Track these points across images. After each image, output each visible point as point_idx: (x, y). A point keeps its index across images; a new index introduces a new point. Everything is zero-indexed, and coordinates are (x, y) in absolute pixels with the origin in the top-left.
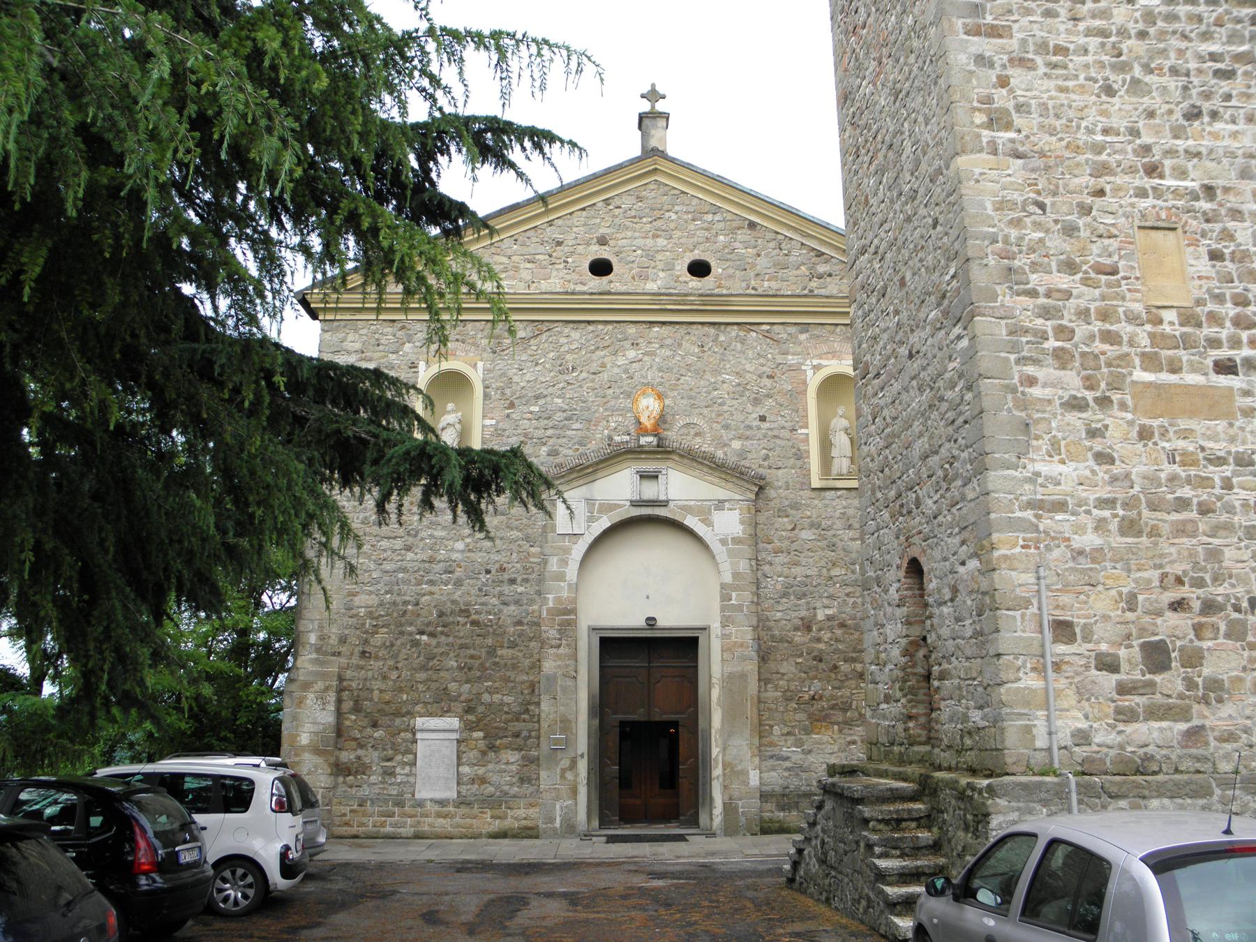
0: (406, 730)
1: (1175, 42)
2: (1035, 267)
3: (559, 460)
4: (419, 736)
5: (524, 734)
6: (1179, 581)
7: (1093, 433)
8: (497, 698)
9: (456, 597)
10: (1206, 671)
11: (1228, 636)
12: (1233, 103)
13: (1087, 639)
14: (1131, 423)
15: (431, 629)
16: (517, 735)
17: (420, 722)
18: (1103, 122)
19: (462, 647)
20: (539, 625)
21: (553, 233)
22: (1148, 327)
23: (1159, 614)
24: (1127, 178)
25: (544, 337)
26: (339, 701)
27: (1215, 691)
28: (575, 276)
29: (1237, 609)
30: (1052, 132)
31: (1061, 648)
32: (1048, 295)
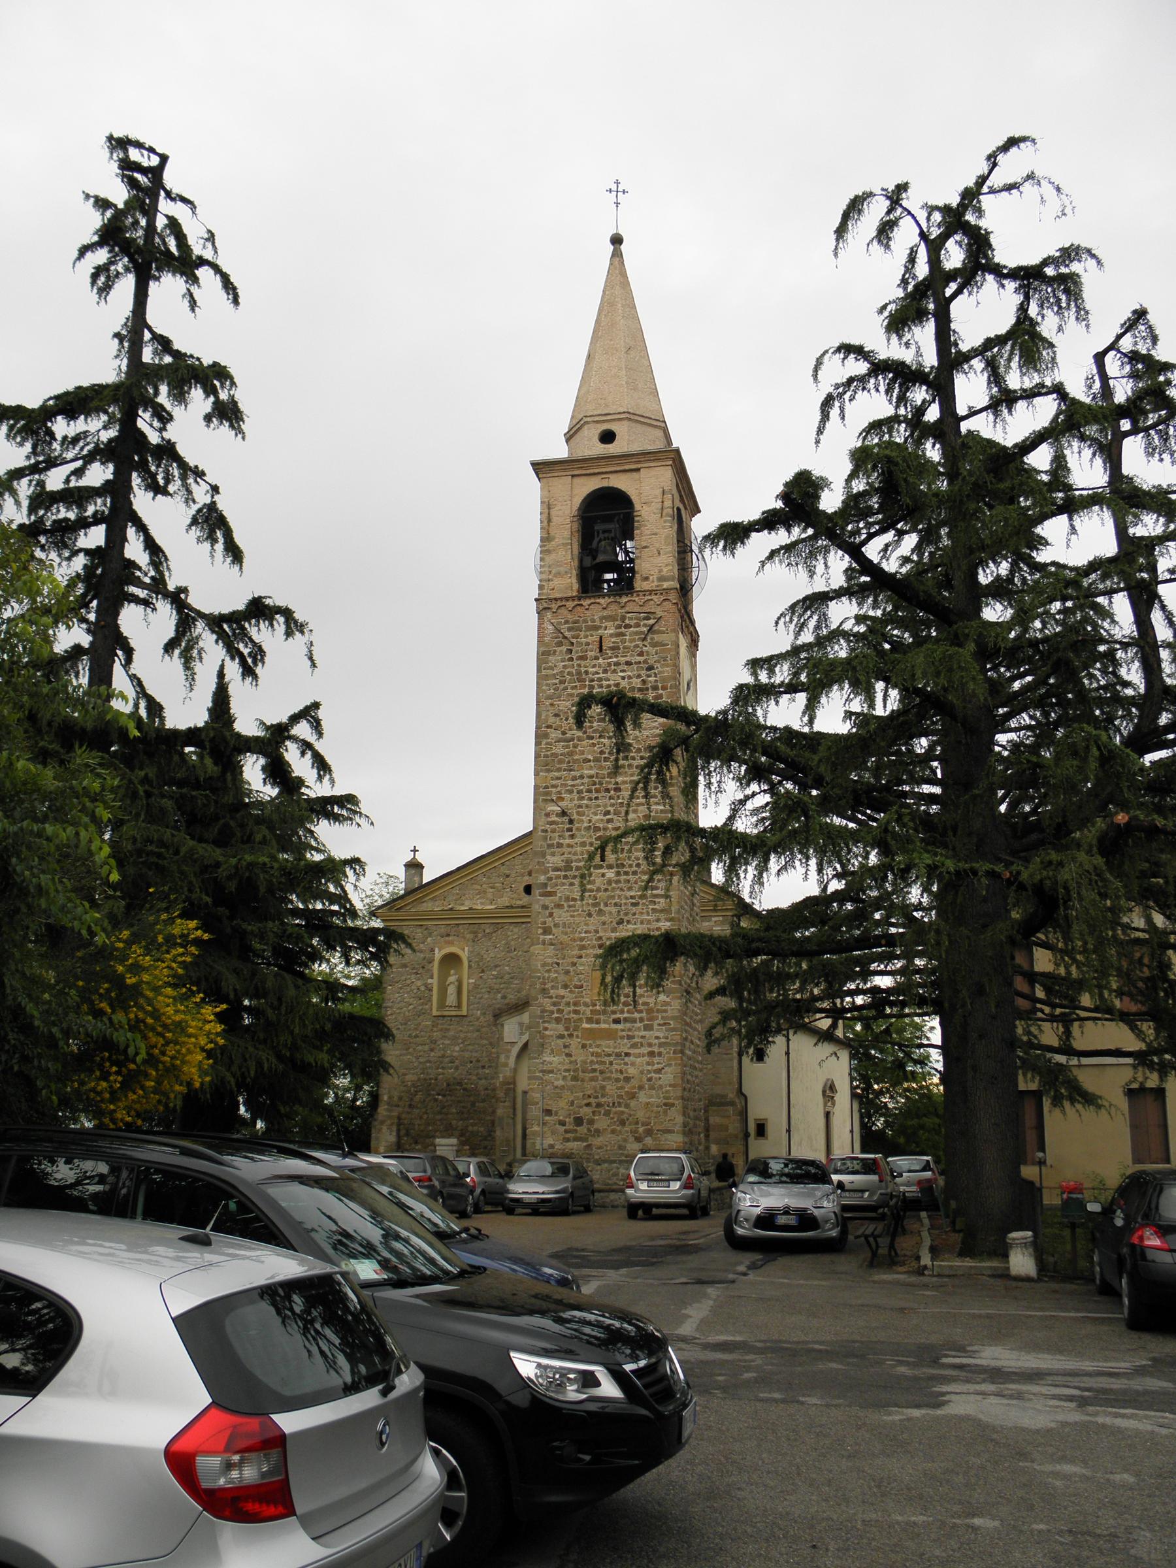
1: (618, 892)
2: (553, 987)
3: (507, 1001)
6: (589, 1097)
7: (565, 1047)
8: (475, 1128)
9: (456, 1075)
16: (485, 1148)
17: (438, 1141)
26: (398, 1131)
27: (598, 1132)
28: (515, 896)
30: (566, 934)
31: (547, 1118)
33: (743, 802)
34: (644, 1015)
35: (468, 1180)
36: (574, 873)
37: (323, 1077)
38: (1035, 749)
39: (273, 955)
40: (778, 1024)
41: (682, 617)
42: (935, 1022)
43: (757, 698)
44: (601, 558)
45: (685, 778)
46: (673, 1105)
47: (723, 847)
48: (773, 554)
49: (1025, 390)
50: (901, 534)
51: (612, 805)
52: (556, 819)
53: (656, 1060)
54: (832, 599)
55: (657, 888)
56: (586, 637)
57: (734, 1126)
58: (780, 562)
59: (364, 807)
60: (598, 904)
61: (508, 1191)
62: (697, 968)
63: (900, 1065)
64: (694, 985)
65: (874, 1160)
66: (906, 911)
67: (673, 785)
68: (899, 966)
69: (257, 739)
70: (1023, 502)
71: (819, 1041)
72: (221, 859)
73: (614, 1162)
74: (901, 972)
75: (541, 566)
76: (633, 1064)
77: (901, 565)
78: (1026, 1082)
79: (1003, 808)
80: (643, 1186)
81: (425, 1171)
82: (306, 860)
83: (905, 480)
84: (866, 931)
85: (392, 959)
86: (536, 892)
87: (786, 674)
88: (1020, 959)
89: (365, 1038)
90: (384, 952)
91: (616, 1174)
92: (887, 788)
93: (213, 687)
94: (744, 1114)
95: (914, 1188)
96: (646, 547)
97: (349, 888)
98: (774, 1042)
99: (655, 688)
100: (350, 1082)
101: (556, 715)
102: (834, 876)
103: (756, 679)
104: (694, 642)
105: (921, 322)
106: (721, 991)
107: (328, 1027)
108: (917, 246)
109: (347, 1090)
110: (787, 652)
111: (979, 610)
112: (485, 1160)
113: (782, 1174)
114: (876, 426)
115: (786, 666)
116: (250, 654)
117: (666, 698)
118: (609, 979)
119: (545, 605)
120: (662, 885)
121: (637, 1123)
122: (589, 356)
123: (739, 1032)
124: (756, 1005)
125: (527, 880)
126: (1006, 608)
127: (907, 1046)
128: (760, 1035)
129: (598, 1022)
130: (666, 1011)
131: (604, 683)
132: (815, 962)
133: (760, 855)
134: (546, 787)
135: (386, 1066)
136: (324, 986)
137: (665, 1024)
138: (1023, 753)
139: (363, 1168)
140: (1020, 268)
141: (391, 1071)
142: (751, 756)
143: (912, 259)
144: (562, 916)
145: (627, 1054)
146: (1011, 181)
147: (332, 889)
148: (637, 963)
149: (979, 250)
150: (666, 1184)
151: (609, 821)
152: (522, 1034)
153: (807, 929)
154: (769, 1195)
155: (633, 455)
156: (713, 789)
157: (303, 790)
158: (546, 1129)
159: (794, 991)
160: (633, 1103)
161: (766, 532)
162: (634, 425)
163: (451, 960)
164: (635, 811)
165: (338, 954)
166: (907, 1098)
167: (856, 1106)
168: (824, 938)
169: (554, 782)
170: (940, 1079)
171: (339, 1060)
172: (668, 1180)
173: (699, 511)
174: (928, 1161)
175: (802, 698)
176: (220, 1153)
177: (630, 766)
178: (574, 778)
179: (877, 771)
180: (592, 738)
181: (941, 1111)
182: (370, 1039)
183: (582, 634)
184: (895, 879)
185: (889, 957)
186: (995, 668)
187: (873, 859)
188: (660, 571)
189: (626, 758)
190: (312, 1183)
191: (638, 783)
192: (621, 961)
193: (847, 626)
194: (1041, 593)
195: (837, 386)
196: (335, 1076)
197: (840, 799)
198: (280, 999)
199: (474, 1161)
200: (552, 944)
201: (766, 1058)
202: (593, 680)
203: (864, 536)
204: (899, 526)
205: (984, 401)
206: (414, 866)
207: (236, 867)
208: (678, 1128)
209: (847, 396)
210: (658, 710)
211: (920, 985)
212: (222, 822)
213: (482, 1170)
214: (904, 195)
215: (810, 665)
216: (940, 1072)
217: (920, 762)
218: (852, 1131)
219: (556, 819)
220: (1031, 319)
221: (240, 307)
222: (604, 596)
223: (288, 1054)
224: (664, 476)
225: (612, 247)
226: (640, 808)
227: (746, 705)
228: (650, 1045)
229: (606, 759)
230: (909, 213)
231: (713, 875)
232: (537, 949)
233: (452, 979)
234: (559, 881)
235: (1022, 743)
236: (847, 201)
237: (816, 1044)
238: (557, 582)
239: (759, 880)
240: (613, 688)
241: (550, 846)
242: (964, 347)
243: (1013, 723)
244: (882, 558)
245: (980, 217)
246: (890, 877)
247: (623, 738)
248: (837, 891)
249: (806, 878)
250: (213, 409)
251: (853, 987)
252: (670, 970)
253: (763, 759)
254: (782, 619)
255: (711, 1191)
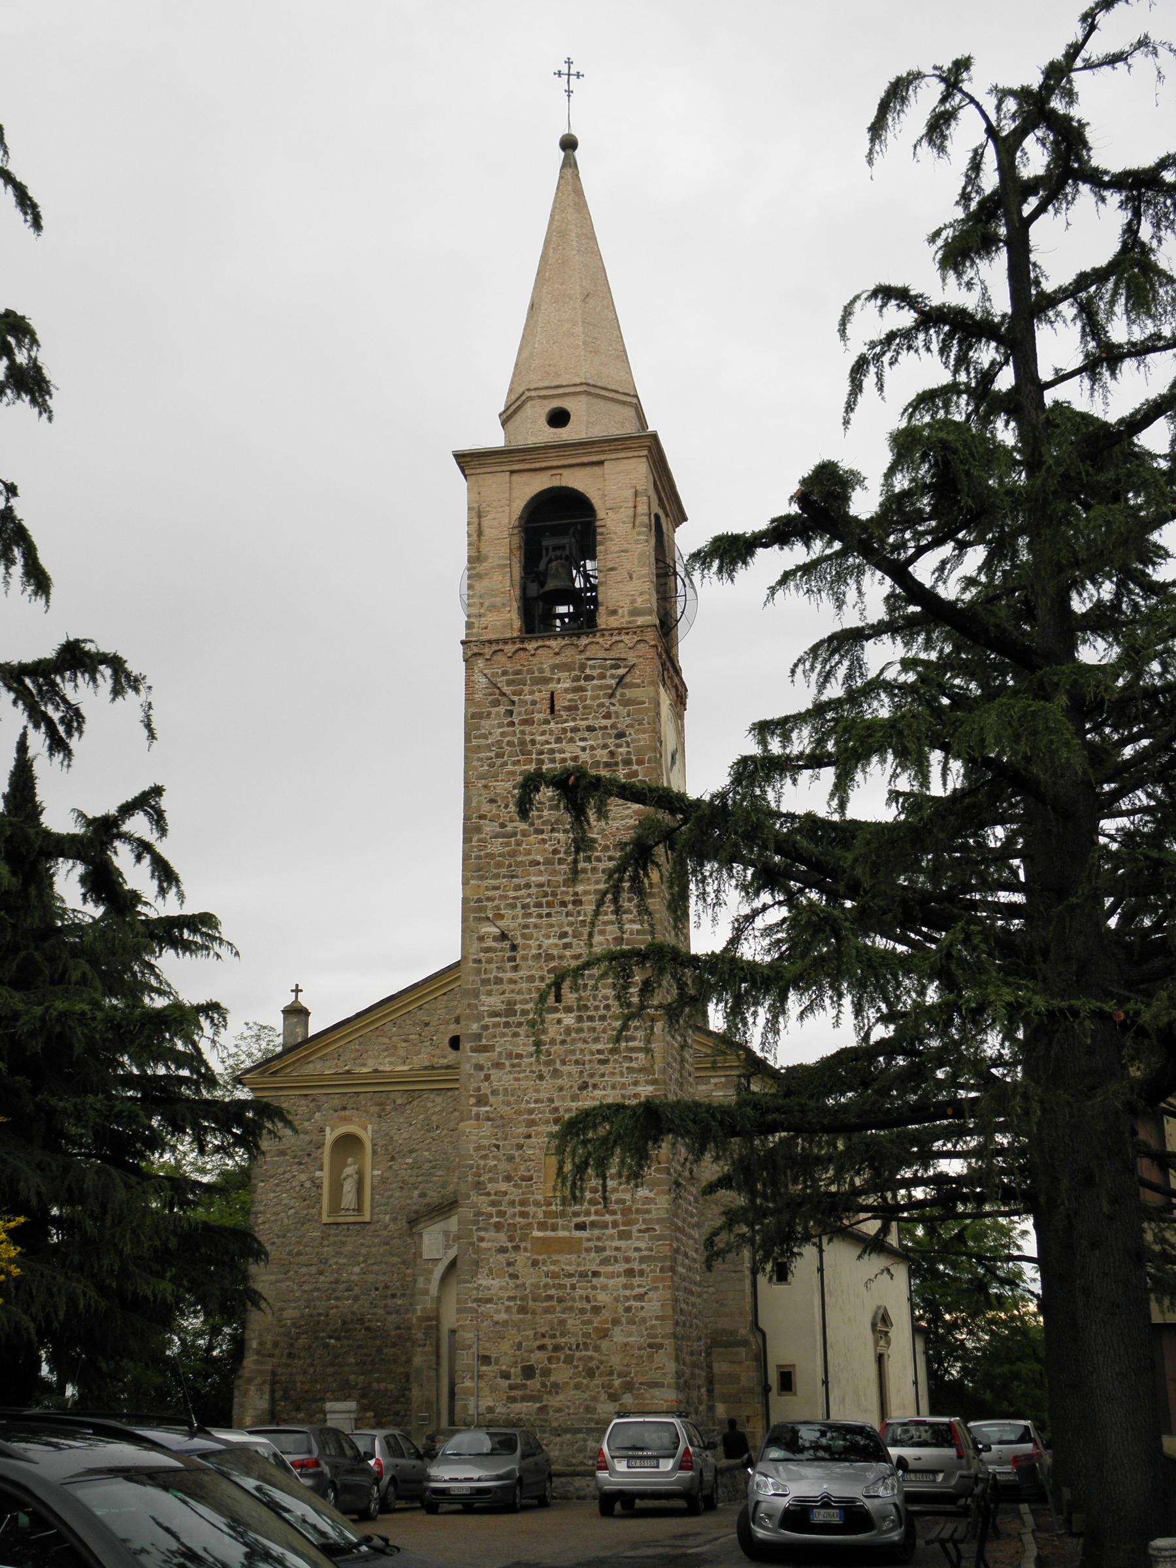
0: (318, 1413)
1: (580, 1045)
2: (491, 1180)
3: (427, 1200)
4: (328, 1416)
5: (402, 1413)
6: (543, 1336)
7: (509, 1264)
9: (354, 1309)
10: (552, 1379)
11: (564, 1362)
12: (606, 1078)
13: (497, 1363)
14: (528, 1258)
15: (337, 1334)
16: (397, 1414)
17: (329, 1406)
18: (535, 1096)
19: (359, 1347)
20: (410, 1328)
21: (422, 1016)
22: (544, 1208)
23: (532, 1351)
24: (544, 1127)
25: (416, 1102)
26: (273, 1392)
27: (556, 1388)
28: (438, 1051)
29: (570, 1349)
30: (508, 1104)
31: (484, 1368)
32: (496, 1194)
33: (750, 918)
34: (618, 1217)
35: (372, 1462)
36: (518, 1018)
37: (165, 1317)
38: (1155, 839)
39: (95, 1141)
40: (806, 1228)
41: (663, 665)
42: (1027, 1224)
43: (767, 775)
44: (551, 585)
45: (671, 887)
46: (661, 1346)
47: (724, 981)
48: (786, 577)
49: (1134, 344)
50: (962, 546)
51: (571, 924)
52: (494, 944)
53: (637, 1281)
54: (868, 638)
55: (633, 1039)
56: (532, 693)
57: (748, 1376)
58: (797, 587)
59: (225, 932)
60: (553, 1062)
61: (429, 1479)
62: (691, 1149)
63: (980, 1286)
64: (687, 1173)
65: (949, 1425)
66: (980, 1068)
67: (652, 895)
68: (973, 1144)
69: (73, 838)
70: (1133, 499)
71: (864, 1252)
72: (21, 1007)
73: (579, 1431)
74: (976, 1153)
75: (469, 597)
76: (604, 1288)
77: (964, 590)
78: (1163, 1312)
79: (1113, 922)
80: (621, 1466)
81: (310, 1452)
82: (143, 1007)
83: (967, 473)
84: (924, 1097)
85: (265, 1144)
86: (466, 1046)
87: (806, 741)
88: (1145, 1134)
89: (226, 1259)
90: (253, 1134)
91: (581, 1450)
92: (950, 897)
93: (10, 764)
94: (761, 1358)
95: (1008, 1468)
96: (612, 569)
97: (204, 1045)
98: (800, 1254)
99: (627, 762)
100: (204, 1323)
101: (492, 801)
102: (878, 1020)
103: (766, 749)
104: (680, 698)
105: (988, 253)
106: (724, 1182)
107: (173, 1243)
108: (983, 146)
109: (198, 1334)
110: (808, 711)
111: (1074, 647)
112: (396, 1432)
113: (816, 1447)
114: (926, 399)
115: (806, 731)
116: (62, 720)
117: (642, 776)
118: (568, 1167)
119: (476, 650)
120: (640, 1034)
121: (611, 1374)
122: (532, 306)
123: (751, 1241)
124: (774, 1201)
125: (453, 1030)
126: (1111, 645)
127: (989, 1259)
128: (781, 1244)
129: (554, 1228)
130: (648, 1211)
131: (558, 756)
132: (855, 1139)
133: (775, 991)
134: (479, 900)
135: (254, 1298)
136: (167, 1184)
137: (647, 1230)
138: (1139, 845)
139: (220, 1452)
140: (1127, 174)
141: (263, 1305)
142: (760, 855)
143: (976, 165)
144: (502, 1079)
145: (596, 1274)
146: (1114, 49)
147: (180, 1046)
148: (606, 1145)
149: (1069, 149)
150: (653, 1462)
151: (567, 946)
152: (447, 1247)
153: (843, 1094)
154: (801, 1478)
155: (593, 443)
156: (709, 901)
157: (140, 908)
158: (482, 1384)
159: (827, 1181)
160: (605, 1344)
161: (776, 547)
162: (594, 401)
163: (348, 1144)
164: (602, 932)
165: (187, 1139)
166: (992, 1333)
167: (920, 1346)
168: (867, 1107)
169: (490, 893)
170: (1038, 1306)
171: (189, 1291)
172: (657, 1458)
173: (685, 519)
174: (1026, 1428)
175: (828, 774)
176: (7, 1440)
177: (594, 869)
178: (518, 888)
179: (935, 873)
180: (542, 832)
181: (1042, 1354)
182: (232, 1259)
183: (526, 689)
184: (963, 1023)
185: (959, 1133)
186: (1098, 728)
187: (932, 996)
188: (633, 602)
189: (588, 859)
190: (143, 1478)
191: (605, 894)
192: (585, 1143)
193: (890, 675)
194: (1160, 624)
195: (872, 345)
196: (182, 1314)
197: (884, 913)
198: (103, 1205)
199: (380, 1434)
200: (489, 1119)
201: (790, 1277)
202: (542, 753)
203: (911, 551)
204: (960, 536)
205: (1078, 361)
206: (296, 1013)
207: (42, 1019)
208: (669, 1380)
209: (886, 359)
210: (630, 793)
211: (1003, 1171)
212: (23, 954)
213: (392, 1447)
214: (965, 75)
215: (839, 729)
216: (1037, 1296)
217: (995, 860)
218: (916, 1383)
219: (494, 944)
220: (1143, 245)
221: (44, 233)
222: (555, 637)
223: (114, 1285)
224: (638, 471)
225: (562, 154)
226: (609, 928)
227: (752, 785)
228: (627, 1260)
229: (561, 862)
230: (972, 100)
231: (711, 1019)
232: (467, 1126)
233: (349, 1170)
234: (498, 1030)
235: (1137, 832)
236: (886, 86)
237: (860, 1257)
238: (491, 619)
239: (773, 1027)
240: (570, 764)
241: (485, 982)
242: (1049, 286)
243: (1125, 805)
244: (937, 580)
245: (1070, 103)
246: (957, 1020)
247: (584, 831)
248: (883, 1040)
249: (837, 1024)
250: (7, 377)
251: (908, 1175)
252: (653, 1153)
253: (777, 858)
254: (801, 667)
255: (718, 1472)
